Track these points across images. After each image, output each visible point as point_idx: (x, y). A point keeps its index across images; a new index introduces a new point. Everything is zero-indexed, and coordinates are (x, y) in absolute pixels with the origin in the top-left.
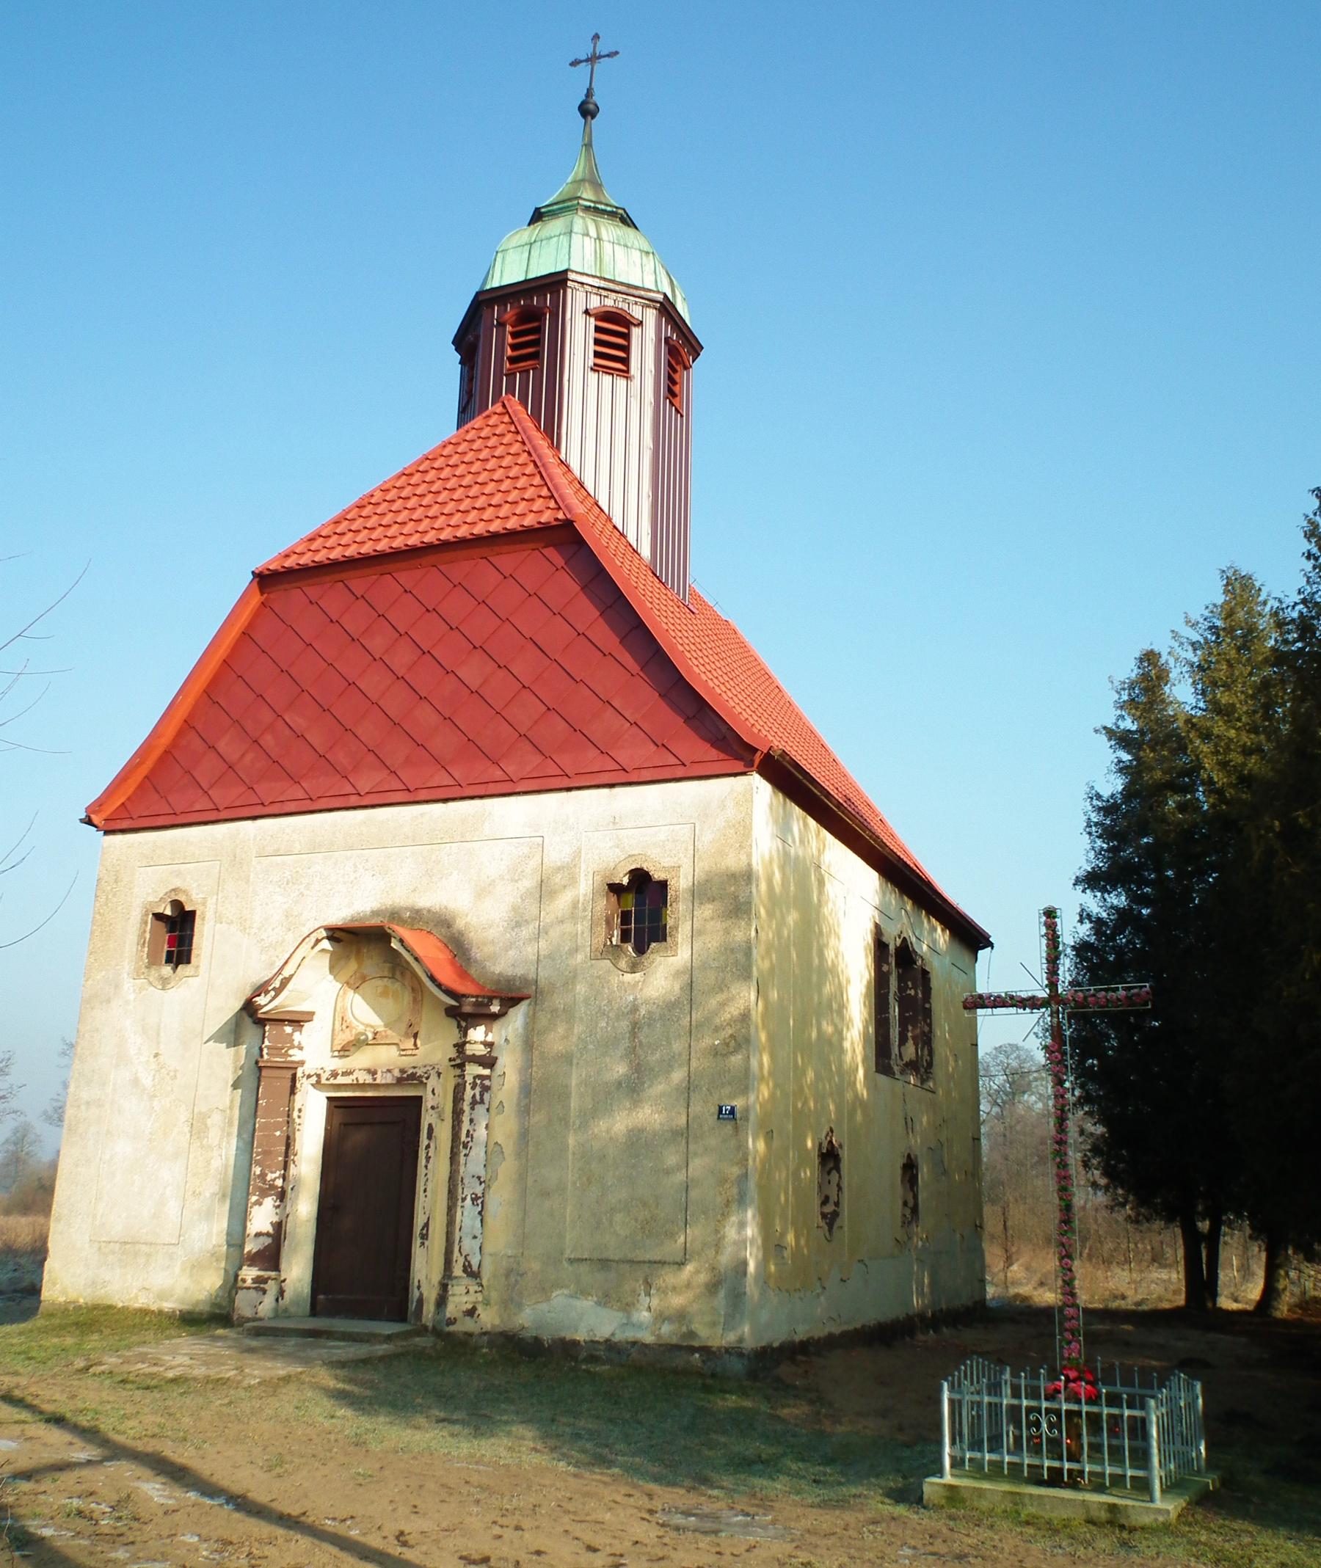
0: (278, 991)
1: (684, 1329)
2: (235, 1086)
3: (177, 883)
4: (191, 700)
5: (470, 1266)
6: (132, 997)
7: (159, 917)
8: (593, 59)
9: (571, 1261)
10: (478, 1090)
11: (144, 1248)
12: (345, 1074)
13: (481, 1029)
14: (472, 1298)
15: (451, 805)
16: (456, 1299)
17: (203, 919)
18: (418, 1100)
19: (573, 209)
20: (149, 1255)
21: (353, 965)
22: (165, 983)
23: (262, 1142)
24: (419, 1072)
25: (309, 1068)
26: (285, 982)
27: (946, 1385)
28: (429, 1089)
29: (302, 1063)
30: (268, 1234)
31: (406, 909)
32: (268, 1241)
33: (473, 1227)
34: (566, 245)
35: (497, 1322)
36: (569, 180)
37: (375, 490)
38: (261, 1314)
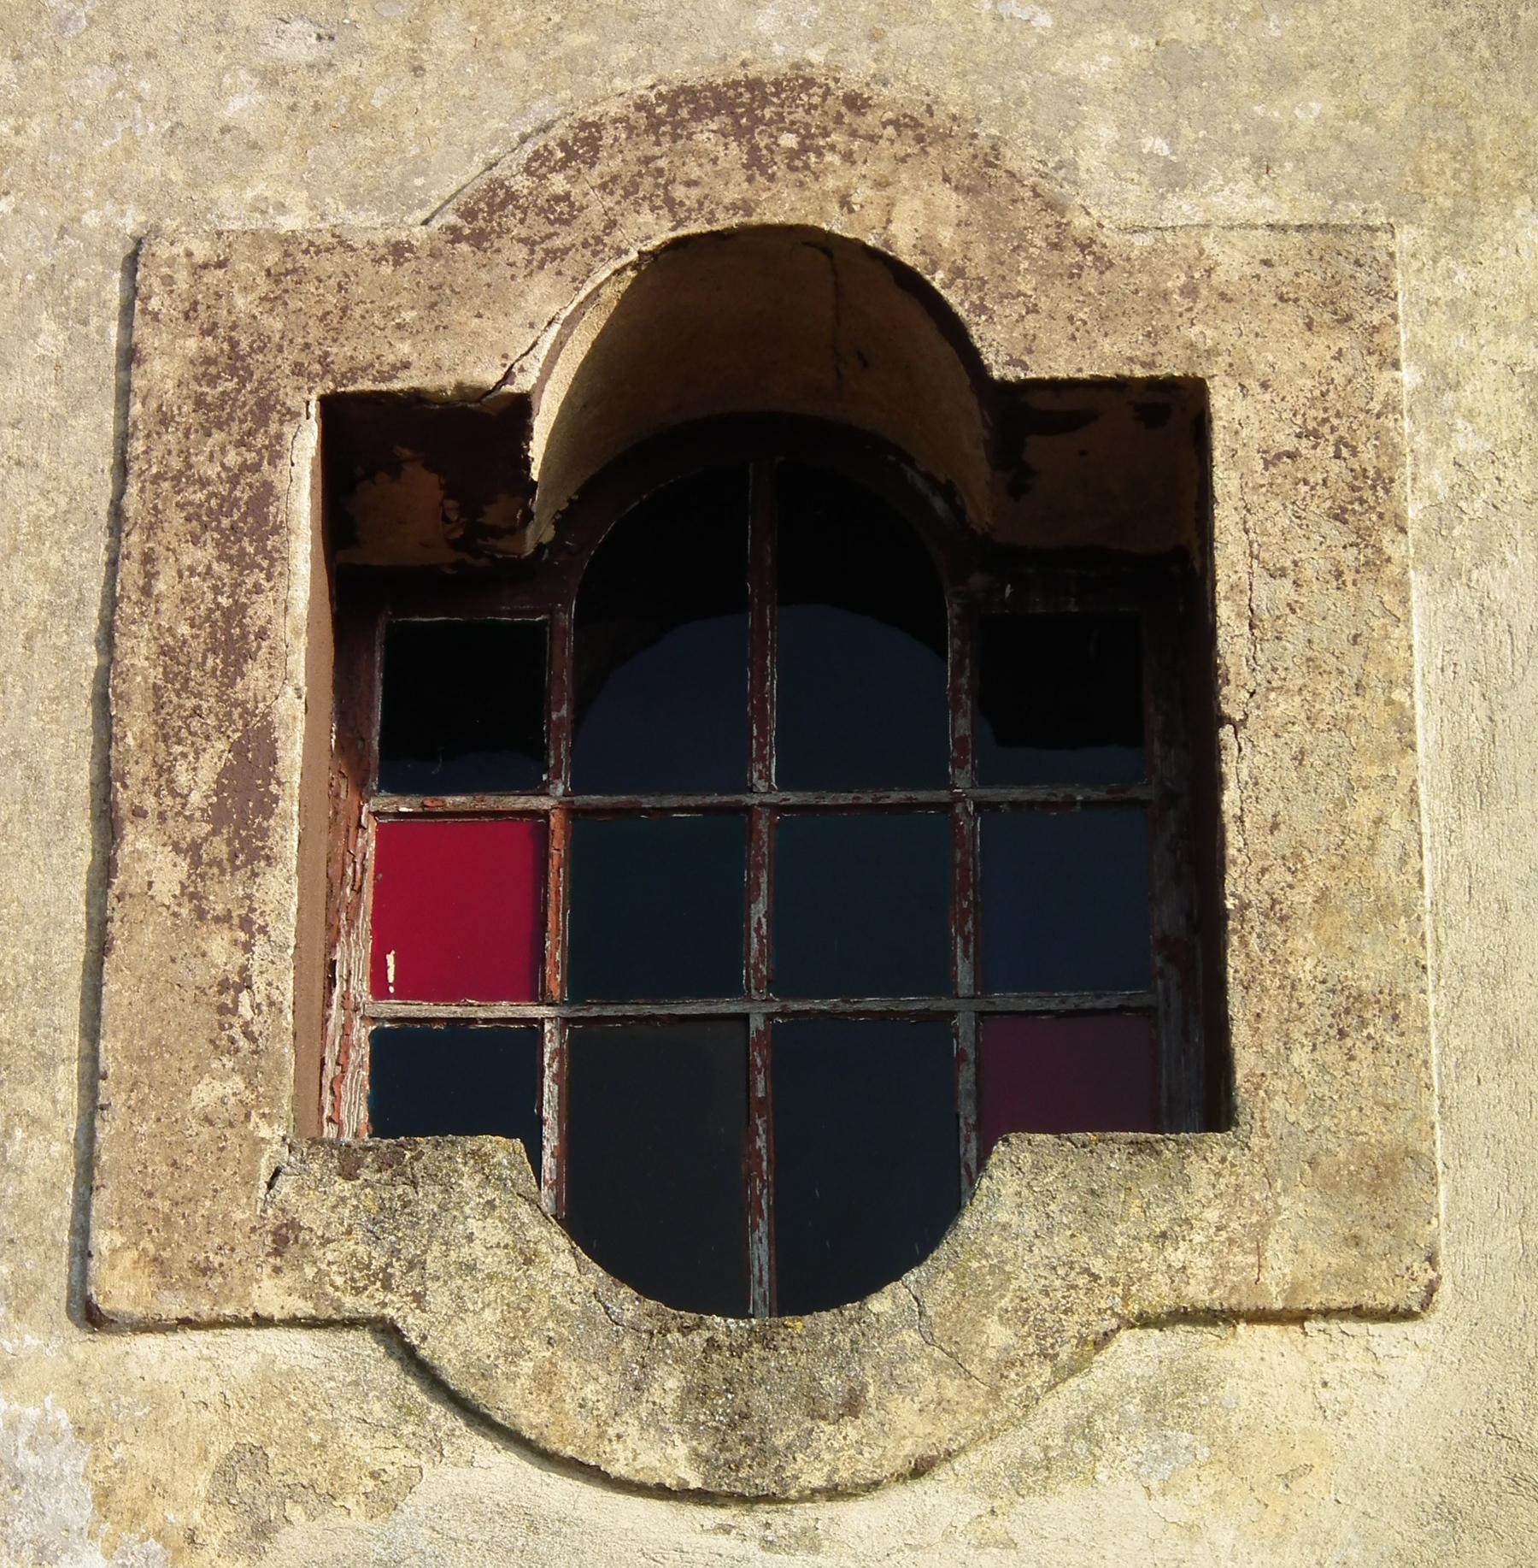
17: (1363, 501)
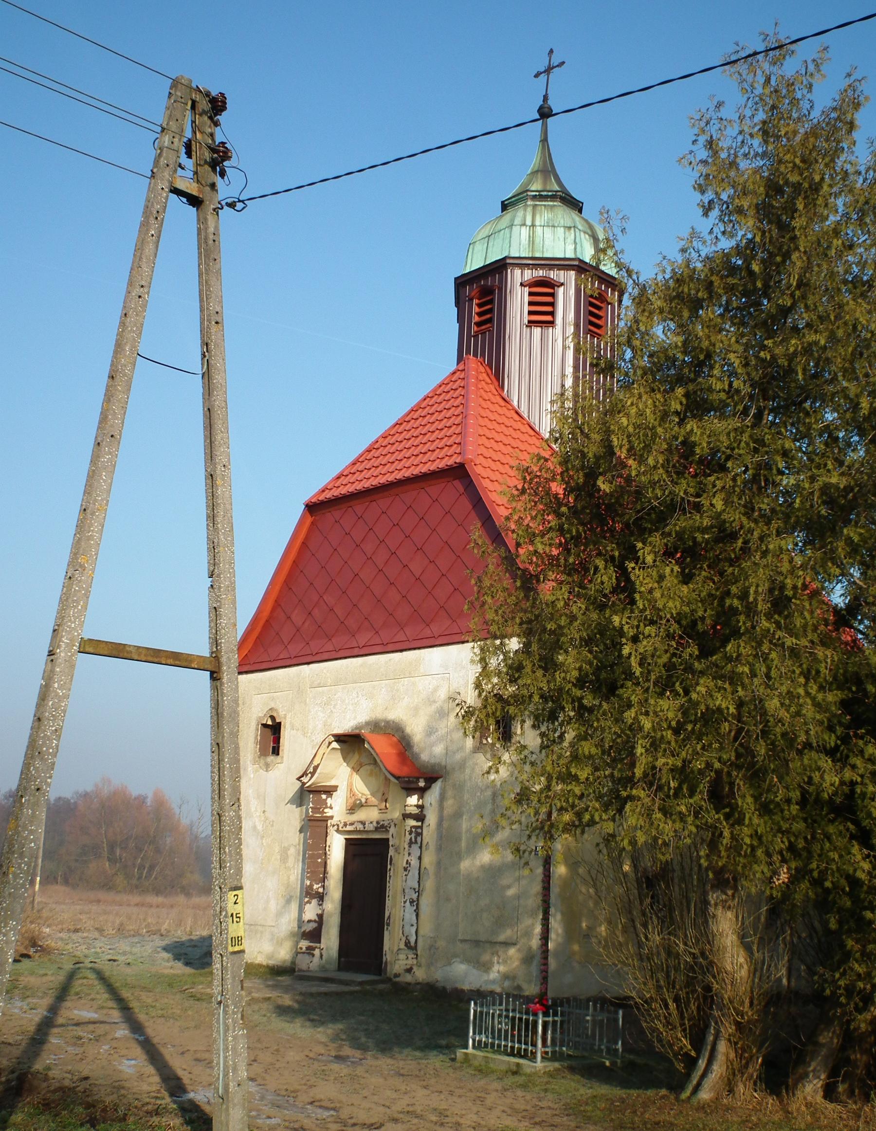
0: (313, 774)
1: (515, 984)
2: (301, 831)
3: (272, 705)
4: (278, 588)
5: (409, 942)
6: (252, 776)
7: (265, 726)
8: (548, 70)
9: (462, 941)
10: (413, 835)
11: (260, 928)
12: (351, 824)
13: (415, 797)
14: (410, 962)
15: (404, 653)
16: (400, 962)
18: (388, 839)
19: (524, 199)
20: (262, 932)
21: (356, 757)
22: (267, 767)
23: (315, 866)
24: (386, 823)
25: (334, 821)
26: (316, 768)
27: (472, 1003)
28: (391, 833)
29: (332, 817)
30: (315, 921)
31: (382, 720)
32: (314, 925)
33: (411, 919)
34: (508, 236)
35: (425, 977)
36: (529, 172)
37: (378, 438)
38: (311, 969)
